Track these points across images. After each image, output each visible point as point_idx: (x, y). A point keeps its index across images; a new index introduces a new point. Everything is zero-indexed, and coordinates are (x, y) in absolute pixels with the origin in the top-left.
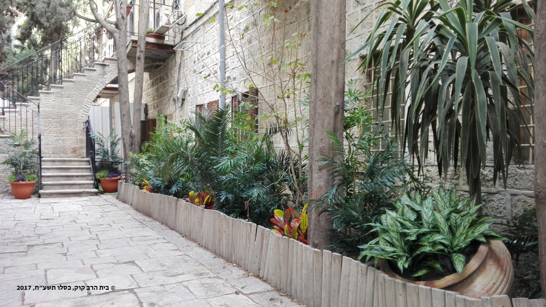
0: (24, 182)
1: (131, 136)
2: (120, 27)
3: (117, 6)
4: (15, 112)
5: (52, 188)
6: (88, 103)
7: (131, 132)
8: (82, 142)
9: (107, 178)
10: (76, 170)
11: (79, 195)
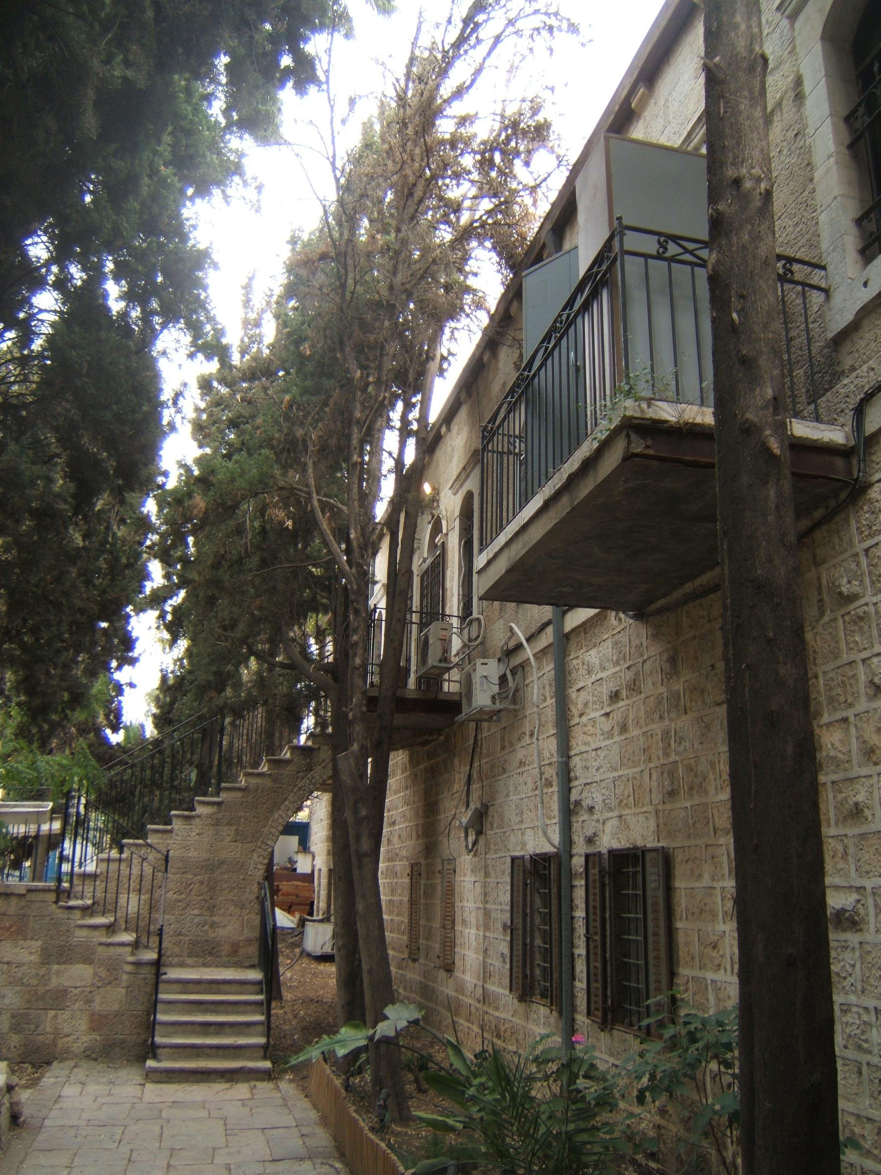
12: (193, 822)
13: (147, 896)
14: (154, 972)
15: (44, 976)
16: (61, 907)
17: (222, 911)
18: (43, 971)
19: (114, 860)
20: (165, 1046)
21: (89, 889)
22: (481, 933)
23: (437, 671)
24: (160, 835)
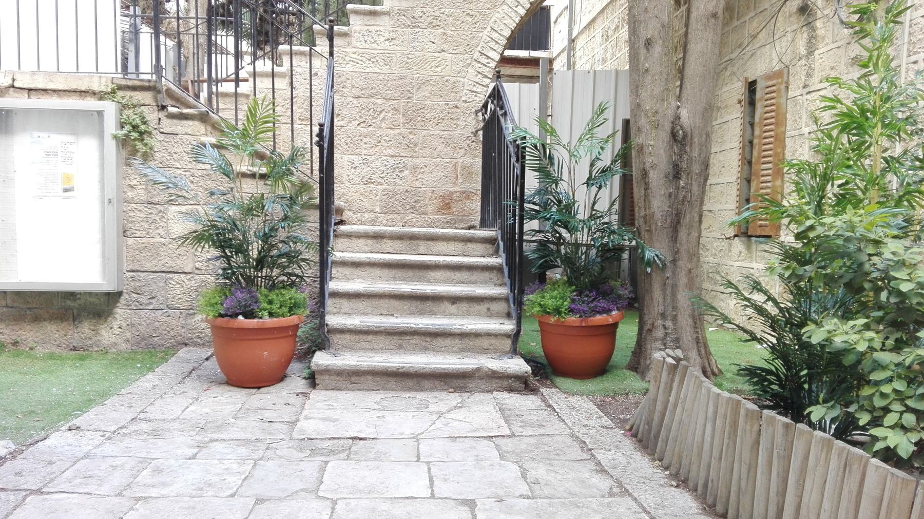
0: (253, 323)
1: (674, 135)
5: (364, 345)
6: (492, 44)
7: (678, 117)
8: (467, 171)
9: (572, 319)
10: (449, 274)
11: (460, 382)
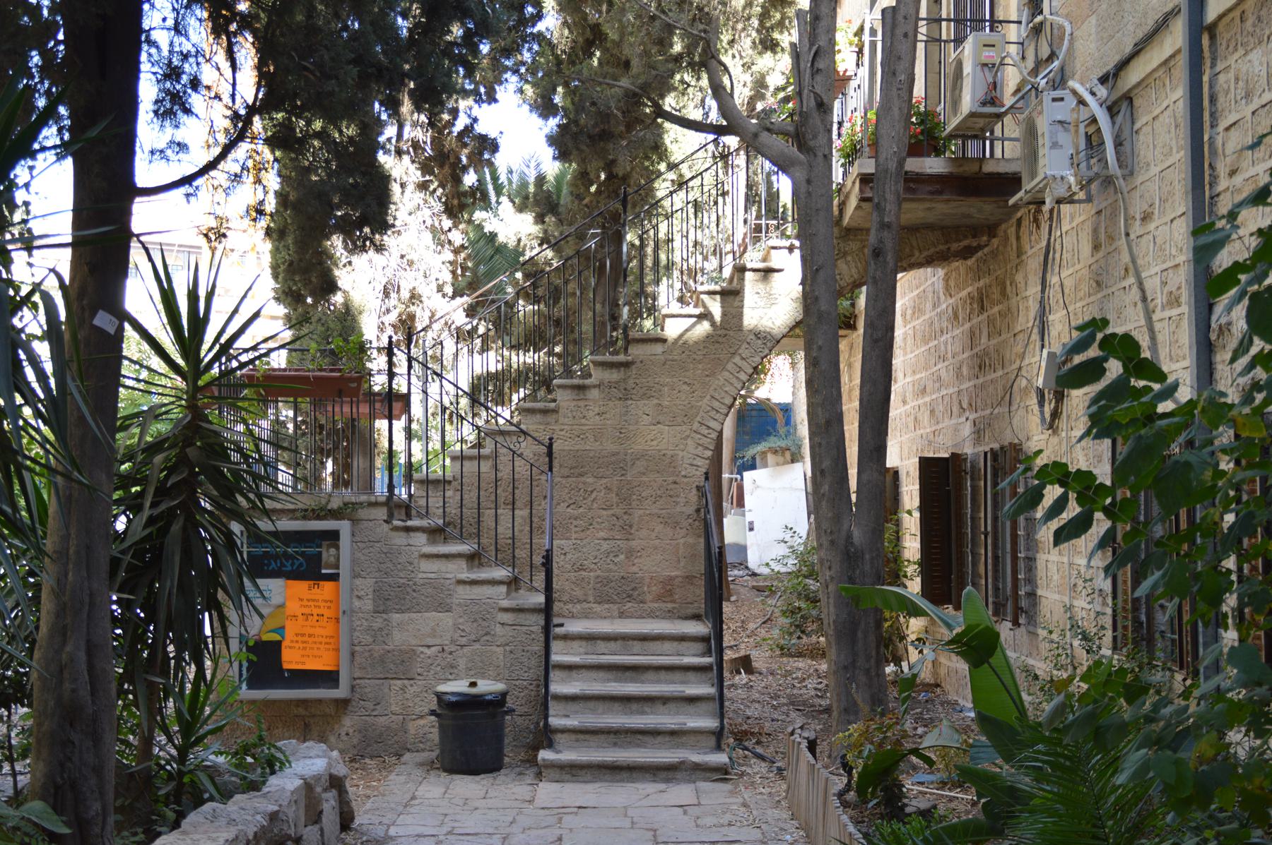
2: (812, 143)
3: (802, 65)
4: (479, 457)
12: (587, 392)
13: (526, 512)
14: (542, 623)
15: (381, 629)
16: (396, 529)
17: (644, 533)
18: (378, 623)
19: (471, 458)
20: (564, 731)
21: (435, 502)
22: (1065, 560)
23: (981, 122)
24: (538, 417)
